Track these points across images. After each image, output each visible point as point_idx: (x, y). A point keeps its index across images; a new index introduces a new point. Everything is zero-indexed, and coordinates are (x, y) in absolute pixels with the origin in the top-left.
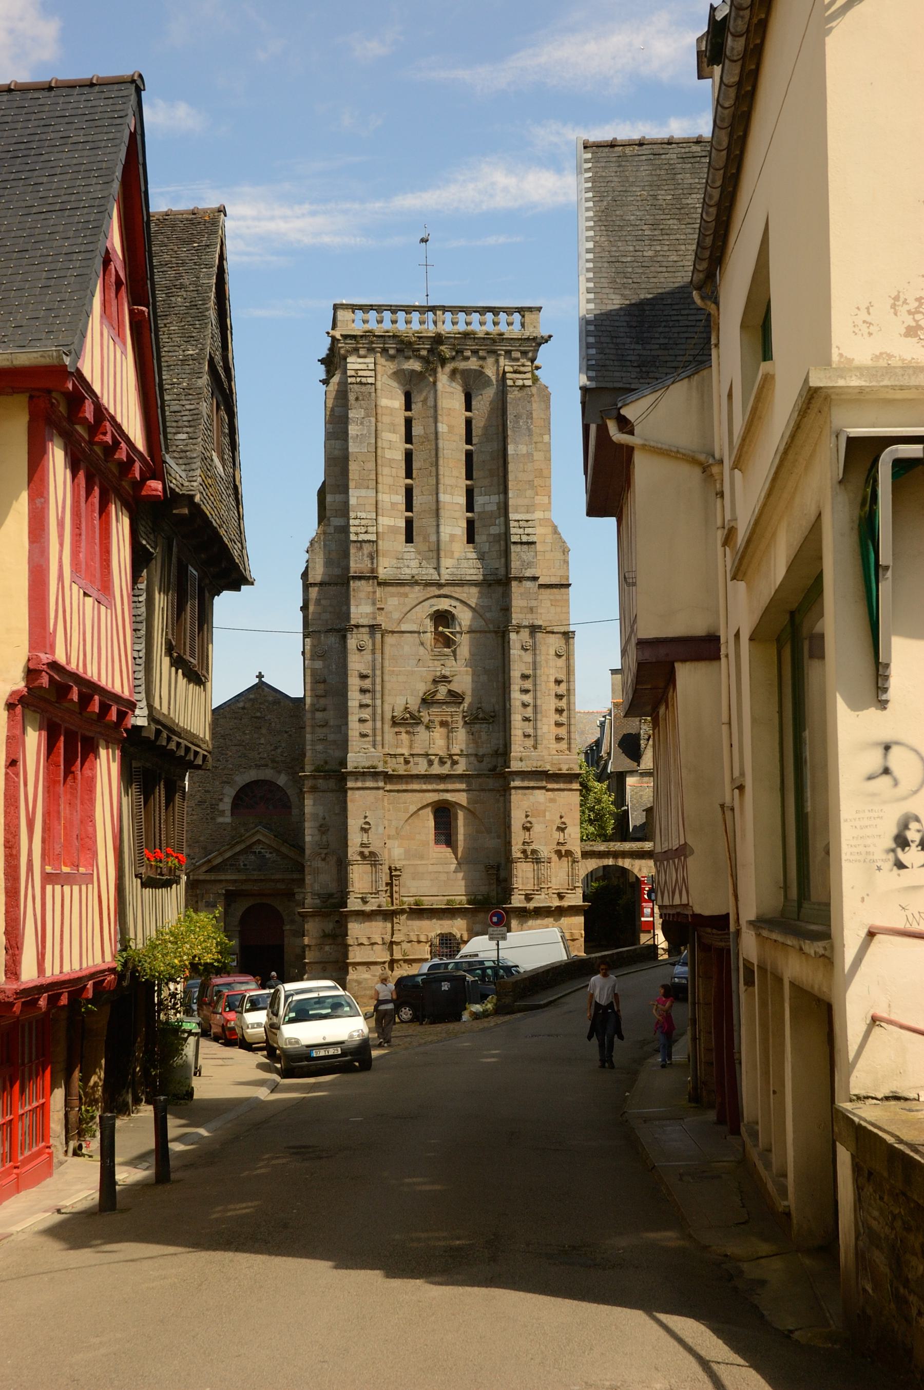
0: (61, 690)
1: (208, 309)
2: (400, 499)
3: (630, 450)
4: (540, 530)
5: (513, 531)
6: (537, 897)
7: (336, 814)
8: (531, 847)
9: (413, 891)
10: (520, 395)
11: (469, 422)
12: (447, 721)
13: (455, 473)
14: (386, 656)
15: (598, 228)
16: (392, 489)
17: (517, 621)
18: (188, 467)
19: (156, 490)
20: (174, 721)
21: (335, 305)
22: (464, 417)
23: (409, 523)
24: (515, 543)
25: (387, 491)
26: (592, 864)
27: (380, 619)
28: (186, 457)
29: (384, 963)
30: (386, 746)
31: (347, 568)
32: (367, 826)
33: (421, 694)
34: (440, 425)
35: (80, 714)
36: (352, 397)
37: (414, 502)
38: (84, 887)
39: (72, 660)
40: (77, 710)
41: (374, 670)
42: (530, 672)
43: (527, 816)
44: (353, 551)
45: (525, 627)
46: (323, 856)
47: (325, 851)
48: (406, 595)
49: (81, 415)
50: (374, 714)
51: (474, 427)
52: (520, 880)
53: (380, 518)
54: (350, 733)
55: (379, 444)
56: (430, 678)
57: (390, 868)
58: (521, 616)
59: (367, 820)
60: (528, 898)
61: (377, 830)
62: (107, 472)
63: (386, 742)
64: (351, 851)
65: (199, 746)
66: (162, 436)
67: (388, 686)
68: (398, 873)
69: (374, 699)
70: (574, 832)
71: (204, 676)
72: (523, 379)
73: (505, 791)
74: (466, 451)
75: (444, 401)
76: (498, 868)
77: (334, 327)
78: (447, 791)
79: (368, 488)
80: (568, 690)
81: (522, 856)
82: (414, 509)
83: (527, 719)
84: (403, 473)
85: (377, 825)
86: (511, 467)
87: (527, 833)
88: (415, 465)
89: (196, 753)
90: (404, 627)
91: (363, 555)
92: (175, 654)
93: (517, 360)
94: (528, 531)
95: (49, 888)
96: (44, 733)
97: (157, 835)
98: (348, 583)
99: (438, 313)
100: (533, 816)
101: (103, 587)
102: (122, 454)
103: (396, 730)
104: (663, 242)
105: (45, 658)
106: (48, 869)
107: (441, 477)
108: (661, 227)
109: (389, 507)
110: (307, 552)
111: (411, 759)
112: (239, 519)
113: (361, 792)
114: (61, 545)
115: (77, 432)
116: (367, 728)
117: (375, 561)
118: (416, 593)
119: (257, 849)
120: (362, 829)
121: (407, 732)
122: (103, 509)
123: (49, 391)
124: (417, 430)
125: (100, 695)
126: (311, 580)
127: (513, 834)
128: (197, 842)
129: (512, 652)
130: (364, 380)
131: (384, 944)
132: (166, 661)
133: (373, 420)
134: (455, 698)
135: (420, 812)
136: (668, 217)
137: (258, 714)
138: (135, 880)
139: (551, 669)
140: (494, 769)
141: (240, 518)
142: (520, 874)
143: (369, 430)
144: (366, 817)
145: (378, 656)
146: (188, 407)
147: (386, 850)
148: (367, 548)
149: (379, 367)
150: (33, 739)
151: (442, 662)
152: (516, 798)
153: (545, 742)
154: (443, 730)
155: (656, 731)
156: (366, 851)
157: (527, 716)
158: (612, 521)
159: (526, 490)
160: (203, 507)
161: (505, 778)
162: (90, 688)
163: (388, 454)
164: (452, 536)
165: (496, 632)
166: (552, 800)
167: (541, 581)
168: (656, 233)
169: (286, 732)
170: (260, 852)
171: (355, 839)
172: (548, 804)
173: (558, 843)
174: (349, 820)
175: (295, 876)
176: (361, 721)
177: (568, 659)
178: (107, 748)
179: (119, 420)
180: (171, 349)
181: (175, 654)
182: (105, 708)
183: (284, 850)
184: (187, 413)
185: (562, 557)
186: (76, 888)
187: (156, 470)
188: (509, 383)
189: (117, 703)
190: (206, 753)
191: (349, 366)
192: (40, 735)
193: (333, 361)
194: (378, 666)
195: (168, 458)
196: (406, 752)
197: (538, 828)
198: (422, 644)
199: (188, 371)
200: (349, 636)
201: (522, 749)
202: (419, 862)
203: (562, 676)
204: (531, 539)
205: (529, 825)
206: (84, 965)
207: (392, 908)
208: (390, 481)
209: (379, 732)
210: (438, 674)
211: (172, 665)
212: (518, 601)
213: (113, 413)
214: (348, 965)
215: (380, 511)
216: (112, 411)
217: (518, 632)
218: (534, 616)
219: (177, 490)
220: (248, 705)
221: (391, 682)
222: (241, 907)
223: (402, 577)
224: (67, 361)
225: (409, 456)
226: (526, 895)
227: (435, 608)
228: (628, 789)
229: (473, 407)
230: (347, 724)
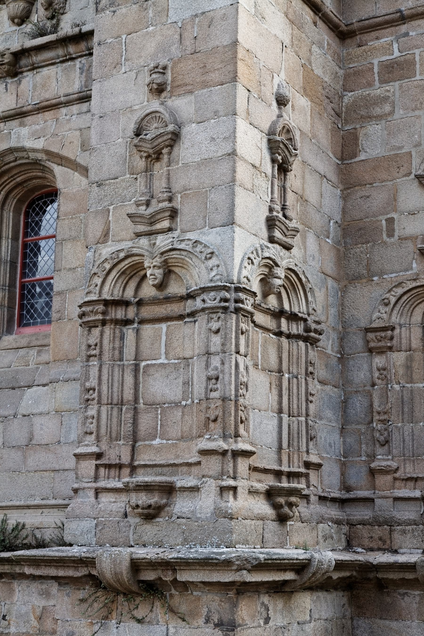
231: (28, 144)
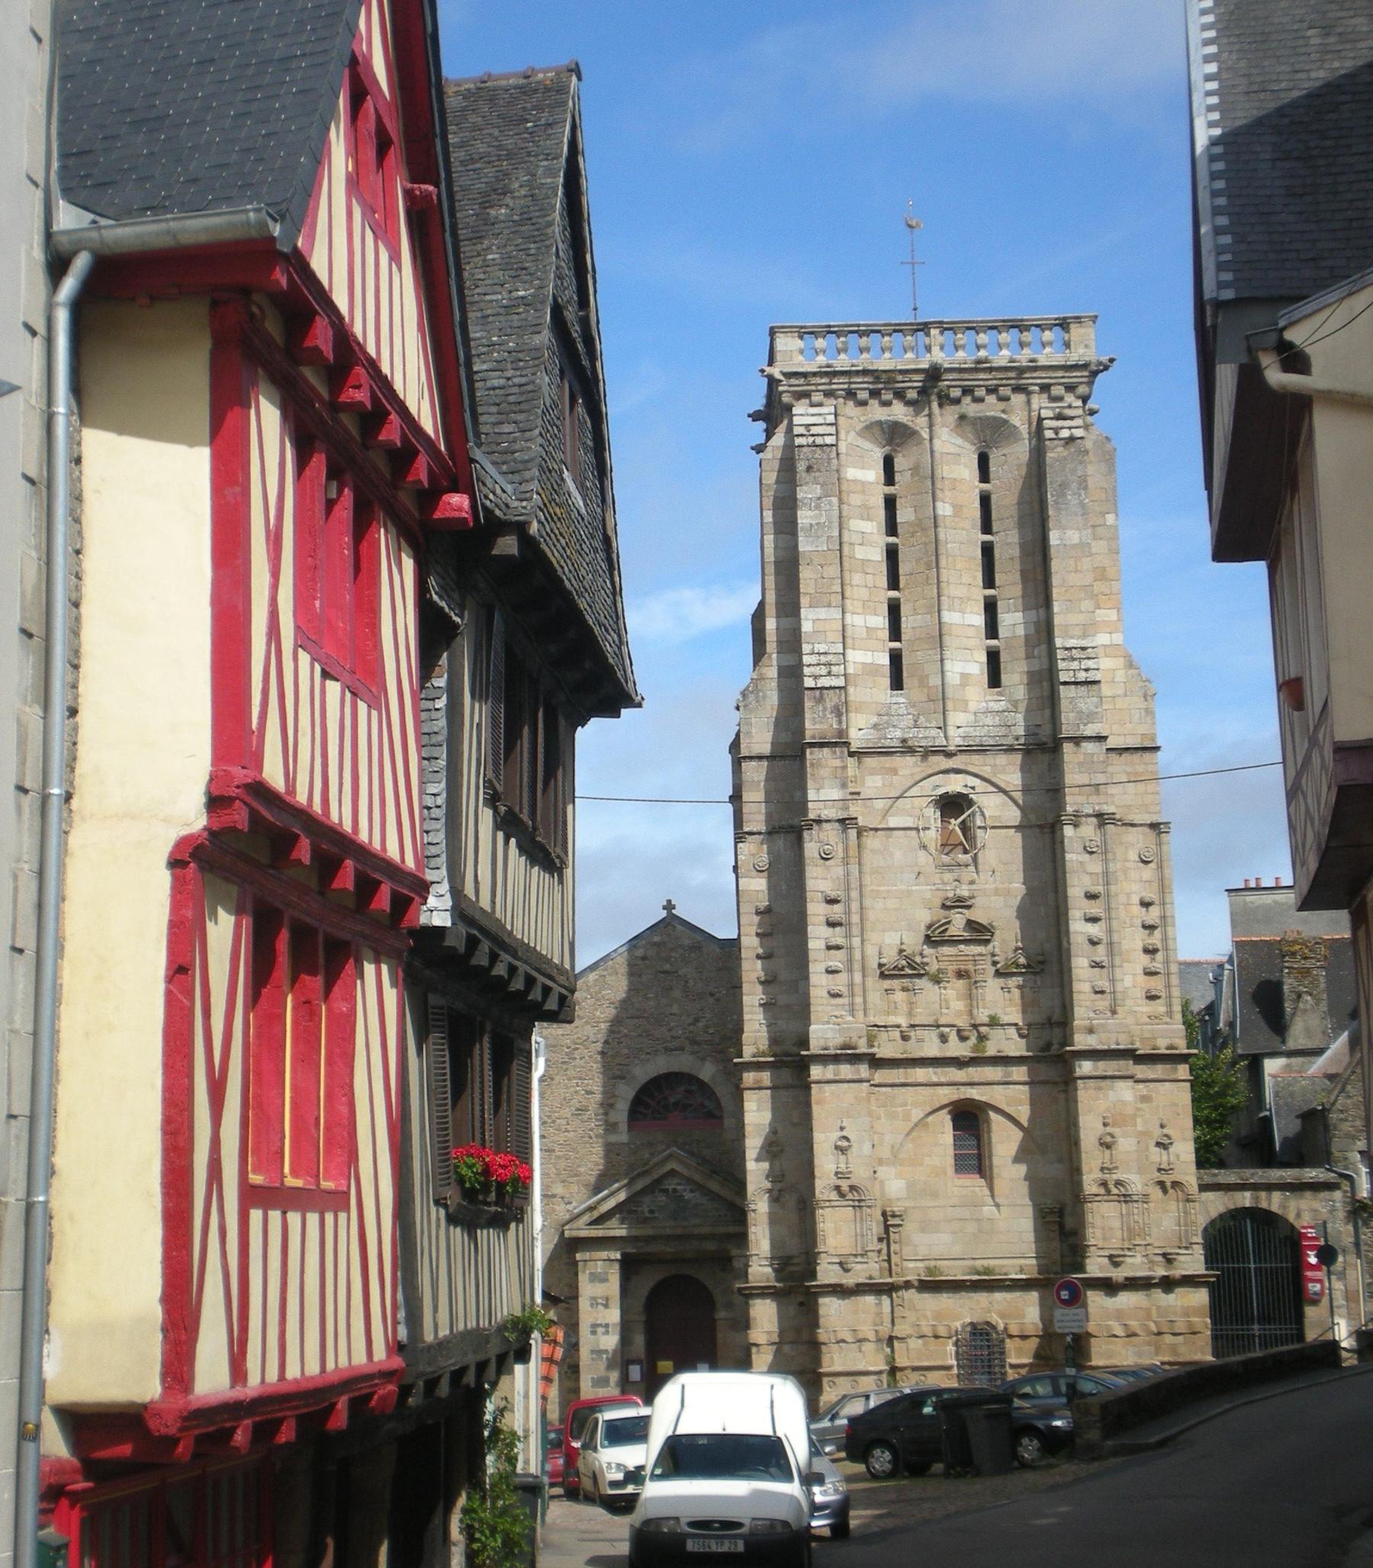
0: (281, 843)
1: (550, 224)
2: (881, 621)
3: (1301, 404)
4: (1105, 663)
5: (1061, 665)
6: (1129, 1260)
7: (794, 1125)
8: (1115, 1177)
9: (923, 1252)
10: (1065, 454)
11: (985, 500)
12: (967, 972)
13: (966, 579)
14: (866, 868)
15: (1225, 40)
16: (867, 608)
17: (1075, 808)
18: (516, 477)
19: (460, 509)
20: (504, 927)
21: (772, 328)
22: (977, 491)
23: (896, 658)
24: (1065, 683)
25: (860, 610)
26: (1216, 1204)
27: (854, 810)
28: (515, 461)
29: (880, 1372)
30: (871, 1012)
31: (801, 731)
32: (845, 1144)
34: (939, 504)
35: (321, 893)
36: (801, 466)
37: (903, 626)
38: (329, 1217)
39: (299, 789)
40: (313, 883)
41: (848, 889)
42: (1100, 889)
43: (1105, 1125)
44: (808, 704)
45: (1088, 816)
46: (776, 1193)
48: (894, 771)
49: (308, 344)
50: (850, 961)
51: (994, 507)
52: (1098, 1233)
53: (850, 653)
54: (813, 992)
55: (845, 538)
56: (938, 902)
57: (884, 1214)
58: (1081, 799)
59: (844, 1133)
60: (1115, 1261)
62: (369, 468)
63: (870, 1005)
65: (551, 978)
66: (467, 416)
67: (871, 915)
68: (896, 1221)
69: (848, 936)
70: (1184, 1151)
71: (558, 857)
72: (1070, 428)
73: (1066, 1083)
74: (983, 543)
75: (945, 468)
76: (1061, 1213)
77: (771, 363)
79: (829, 606)
80: (1163, 917)
81: (1102, 1191)
82: (904, 637)
83: (1097, 965)
84: (883, 581)
86: (1055, 565)
88: (903, 569)
89: (547, 990)
90: (893, 822)
91: (825, 709)
92: (503, 809)
93: (1060, 399)
94: (1090, 664)
95: (256, 1215)
96: (247, 922)
97: (478, 1130)
98: (803, 754)
99: (934, 332)
100: (1114, 1125)
101: (361, 675)
102: (392, 433)
104: (1343, 54)
105: (241, 775)
106: (256, 1179)
107: (943, 585)
108: (1340, 30)
109: (864, 635)
110: (738, 708)
111: (912, 1034)
112: (614, 594)
113: (833, 1086)
114: (275, 574)
115: (306, 381)
116: (840, 982)
117: (844, 718)
118: (908, 765)
119: (671, 1185)
120: (837, 1147)
121: (904, 989)
122: (361, 529)
123: (246, 292)
124: (904, 515)
125: (357, 860)
126: (744, 752)
127: (1084, 1156)
128: (576, 1175)
129: (1068, 856)
130: (819, 441)
131: (879, 1340)
132: (487, 816)
133: (835, 500)
134: (979, 932)
135: (930, 1118)
136: (1352, 13)
137: (668, 967)
138: (433, 1209)
139: (1134, 883)
140: (1048, 1046)
141: (616, 592)
142: (1098, 1221)
143: (828, 518)
144: (842, 1129)
145: (854, 869)
146: (516, 380)
147: (877, 1187)
148: (831, 699)
149: (841, 420)
150: (222, 931)
152: (1085, 1094)
153: (1129, 1002)
154: (961, 984)
155: (1361, 933)
156: (845, 1185)
157: (1098, 960)
158: (1258, 569)
159: (1080, 600)
160: (543, 546)
161: (1065, 1062)
162: (336, 847)
163: (860, 553)
164: (965, 677)
165: (1040, 826)
166: (1145, 1099)
167: (1111, 743)
168: (1331, 40)
169: (712, 995)
170: (675, 1190)
171: (826, 1164)
172: (1140, 1105)
173: (1159, 1170)
174: (815, 1134)
175: (732, 1229)
176: (831, 972)
177: (1160, 867)
178: (377, 962)
179: (385, 369)
180: (488, 289)
181: (503, 809)
182: (367, 887)
183: (714, 1186)
184: (515, 390)
185: (1144, 705)
186: (313, 1218)
187: (456, 474)
188: (1049, 434)
189: (391, 878)
190: (565, 992)
191: (796, 420)
192: (238, 926)
193: (773, 413)
194: (854, 884)
195: (477, 454)
196: (903, 1021)
197: (1126, 1144)
198: (925, 847)
199: (516, 324)
200: (806, 834)
201: (1092, 1015)
202: (933, 1204)
203: (1150, 895)
204: (1092, 676)
205: (1108, 1139)
206: (330, 1365)
207: (889, 1280)
208: (864, 593)
209: (858, 990)
211: (497, 826)
212: (1073, 775)
213: (373, 354)
214: (820, 1376)
215: (849, 641)
216: (371, 350)
217: (1076, 826)
218: (1102, 799)
219: (498, 512)
220: (651, 953)
221: (877, 909)
222: (645, 1283)
223: (888, 743)
224: (276, 230)
225: (892, 554)
226: (1111, 1257)
227: (941, 791)
228: (1268, 1081)
229: (992, 476)
230: (807, 978)
231: (977, 1098)
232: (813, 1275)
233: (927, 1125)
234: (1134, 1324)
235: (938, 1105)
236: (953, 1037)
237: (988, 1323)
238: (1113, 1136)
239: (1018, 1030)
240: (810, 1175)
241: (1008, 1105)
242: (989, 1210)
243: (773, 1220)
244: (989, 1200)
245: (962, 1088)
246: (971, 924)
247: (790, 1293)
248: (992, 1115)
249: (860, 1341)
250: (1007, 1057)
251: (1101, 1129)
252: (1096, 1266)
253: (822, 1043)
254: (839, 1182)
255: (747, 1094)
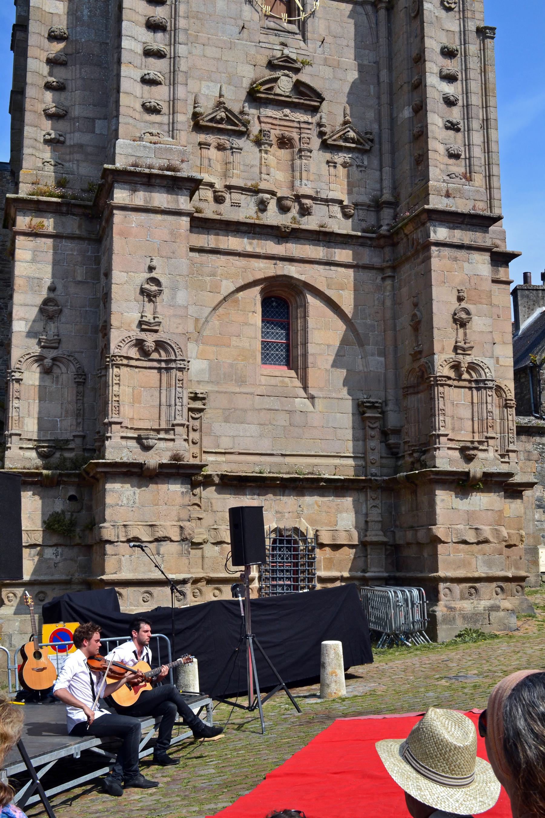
6: (481, 455)
8: (468, 359)
12: (290, 140)
32: (154, 288)
33: (246, 84)
43: (460, 299)
46: (48, 362)
47: (53, 353)
59: (153, 275)
60: (467, 453)
61: (174, 297)
64: (116, 337)
78: (291, 260)
81: (452, 374)
85: (174, 289)
87: (461, 331)
100: (470, 301)
103: (202, 137)
111: (227, 196)
113: (143, 216)
120: (143, 291)
121: (220, 148)
134: (307, 98)
135: (241, 295)
142: (449, 410)
144: (151, 269)
151: (282, 40)
152: (439, 260)
154: (284, 154)
156: (150, 339)
171: (126, 313)
176: (147, 81)
202: (237, 390)
205: (463, 316)
210: (278, 54)
231: (296, 276)
232: (100, 451)
233: (237, 301)
234: (487, 532)
235: (251, 279)
236: (272, 206)
237: (296, 530)
238: (468, 313)
239: (343, 208)
240: (104, 329)
241: (328, 287)
242: (302, 403)
243: (44, 395)
244: (302, 393)
245: (280, 264)
246: (300, 88)
247: (58, 484)
248: (310, 299)
249: (157, 540)
250: (332, 234)
251: (455, 305)
252: (446, 460)
253: (132, 160)
254: (143, 336)
255: (20, 241)
